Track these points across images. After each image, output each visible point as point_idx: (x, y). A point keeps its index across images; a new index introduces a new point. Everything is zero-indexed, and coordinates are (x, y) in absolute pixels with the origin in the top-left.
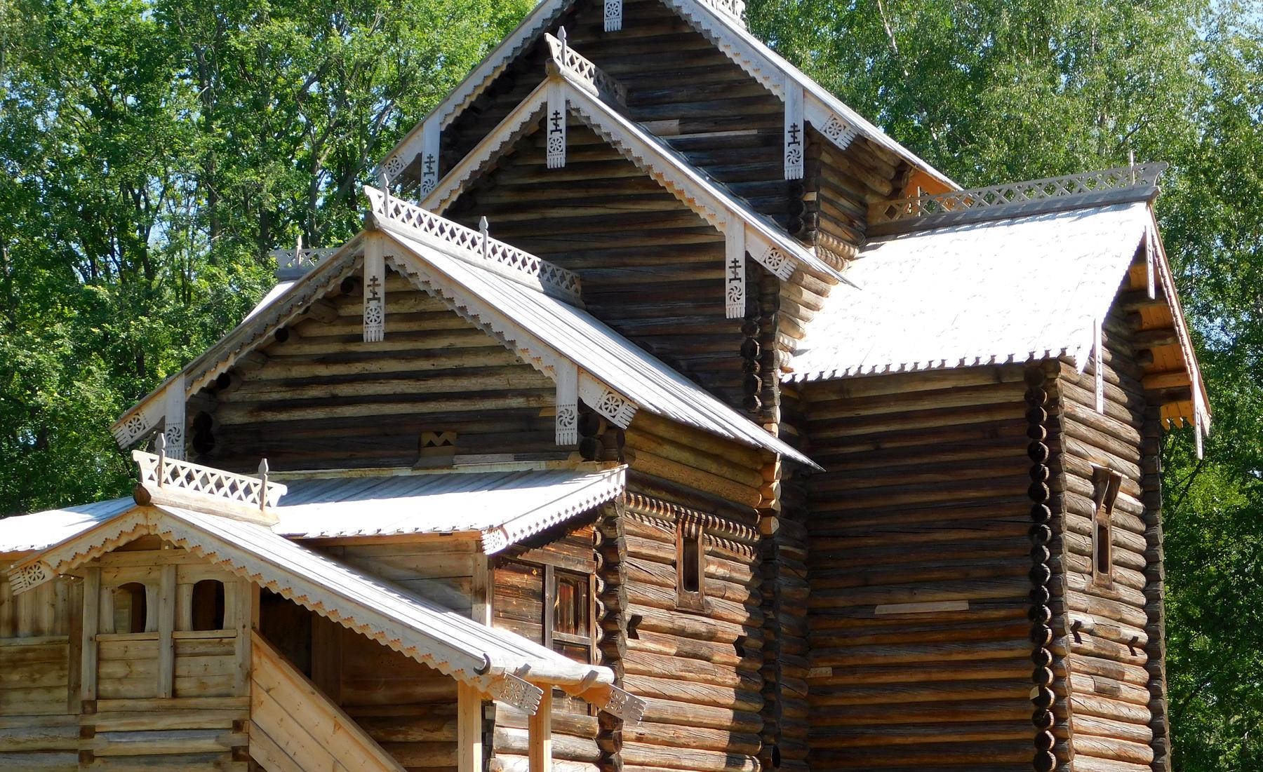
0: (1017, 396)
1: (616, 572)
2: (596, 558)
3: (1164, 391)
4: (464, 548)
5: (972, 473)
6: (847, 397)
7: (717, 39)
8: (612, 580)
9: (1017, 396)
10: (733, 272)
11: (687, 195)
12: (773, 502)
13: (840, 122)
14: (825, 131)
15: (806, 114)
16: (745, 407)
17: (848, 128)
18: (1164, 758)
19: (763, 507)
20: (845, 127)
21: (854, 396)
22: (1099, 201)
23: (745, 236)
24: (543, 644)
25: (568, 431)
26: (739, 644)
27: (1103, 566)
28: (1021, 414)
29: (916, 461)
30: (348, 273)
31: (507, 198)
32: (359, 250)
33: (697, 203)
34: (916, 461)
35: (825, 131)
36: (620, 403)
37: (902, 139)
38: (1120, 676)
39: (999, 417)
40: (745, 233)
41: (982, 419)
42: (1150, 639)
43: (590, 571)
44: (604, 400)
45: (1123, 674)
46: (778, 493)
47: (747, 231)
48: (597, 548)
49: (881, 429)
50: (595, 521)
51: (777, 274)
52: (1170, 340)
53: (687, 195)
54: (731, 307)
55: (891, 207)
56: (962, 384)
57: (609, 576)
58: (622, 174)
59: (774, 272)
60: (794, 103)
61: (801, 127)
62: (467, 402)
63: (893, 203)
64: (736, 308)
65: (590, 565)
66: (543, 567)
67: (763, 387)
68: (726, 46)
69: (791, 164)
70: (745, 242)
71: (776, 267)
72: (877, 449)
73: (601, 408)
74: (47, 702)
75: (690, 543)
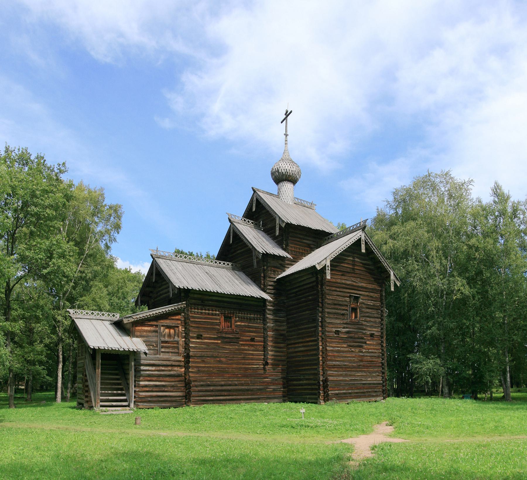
9: (314, 279)
28: (314, 284)
38: (365, 343)
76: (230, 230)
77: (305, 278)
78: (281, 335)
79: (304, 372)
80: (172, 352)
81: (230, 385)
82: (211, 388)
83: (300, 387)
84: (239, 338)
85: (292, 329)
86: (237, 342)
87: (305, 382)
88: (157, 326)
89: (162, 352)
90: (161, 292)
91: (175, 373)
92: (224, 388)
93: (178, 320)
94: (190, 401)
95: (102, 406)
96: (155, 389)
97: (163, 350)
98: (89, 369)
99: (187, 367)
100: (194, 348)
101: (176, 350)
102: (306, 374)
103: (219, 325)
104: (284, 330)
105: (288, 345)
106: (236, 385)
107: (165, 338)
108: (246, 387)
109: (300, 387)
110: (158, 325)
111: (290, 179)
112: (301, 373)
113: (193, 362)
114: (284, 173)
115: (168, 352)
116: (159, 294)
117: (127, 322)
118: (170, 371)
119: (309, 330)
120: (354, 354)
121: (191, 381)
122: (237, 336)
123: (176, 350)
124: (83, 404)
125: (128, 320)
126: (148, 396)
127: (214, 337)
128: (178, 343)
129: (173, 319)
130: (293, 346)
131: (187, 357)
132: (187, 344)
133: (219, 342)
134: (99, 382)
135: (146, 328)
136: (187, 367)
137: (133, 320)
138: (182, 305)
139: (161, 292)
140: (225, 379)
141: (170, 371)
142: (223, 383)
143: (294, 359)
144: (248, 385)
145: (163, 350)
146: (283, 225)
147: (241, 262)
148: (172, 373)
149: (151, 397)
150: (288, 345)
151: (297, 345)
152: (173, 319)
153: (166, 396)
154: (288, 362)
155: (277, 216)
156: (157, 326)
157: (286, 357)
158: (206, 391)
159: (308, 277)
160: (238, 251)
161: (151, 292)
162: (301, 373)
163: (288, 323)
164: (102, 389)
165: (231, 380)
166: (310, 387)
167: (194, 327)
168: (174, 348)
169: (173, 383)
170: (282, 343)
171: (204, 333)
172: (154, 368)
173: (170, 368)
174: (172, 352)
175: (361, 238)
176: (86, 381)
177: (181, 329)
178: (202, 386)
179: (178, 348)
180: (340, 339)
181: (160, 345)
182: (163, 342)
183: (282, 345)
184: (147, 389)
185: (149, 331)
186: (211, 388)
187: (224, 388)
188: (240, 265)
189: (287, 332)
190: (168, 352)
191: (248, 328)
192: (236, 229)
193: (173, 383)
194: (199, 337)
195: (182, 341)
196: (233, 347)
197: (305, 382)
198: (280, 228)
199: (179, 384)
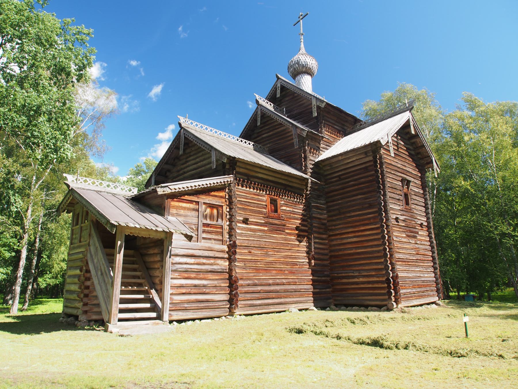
5: (363, 180)
9: (371, 158)
16: (300, 170)
18: (435, 254)
21: (334, 166)
26: (297, 228)
27: (407, 203)
28: (372, 163)
31: (256, 135)
37: (432, 165)
38: (417, 233)
39: (368, 165)
42: (428, 224)
45: (418, 232)
49: (340, 173)
52: (424, 149)
58: (276, 124)
62: (354, 228)
67: (305, 164)
72: (340, 178)
74: (103, 263)
75: (274, 202)
76: (257, 112)
77: (354, 159)
78: (323, 224)
79: (360, 268)
80: (215, 240)
81: (278, 284)
82: (259, 288)
83: (353, 286)
84: (284, 226)
85: (336, 218)
86: (284, 230)
87: (361, 279)
88: (197, 203)
89: (204, 238)
90: (186, 170)
91: (219, 267)
92: (272, 288)
93: (221, 197)
94: (237, 306)
95: (120, 320)
96: (193, 291)
97: (204, 235)
98: (95, 261)
99: (231, 260)
100: (241, 235)
101: (220, 237)
102: (362, 270)
103: (265, 208)
104: (324, 219)
105: (330, 236)
106: (284, 284)
107: (207, 220)
108: (294, 287)
109: (353, 286)
110: (199, 202)
111: (309, 71)
112: (354, 268)
113: (241, 254)
114: (304, 65)
115: (210, 239)
116: (181, 172)
117: (162, 193)
118: (211, 264)
119: (366, 217)
120: (411, 246)
121: (238, 279)
122: (283, 222)
123: (220, 237)
124: (76, 317)
125: (164, 191)
126: (184, 301)
127: (261, 223)
128: (222, 227)
129: (216, 196)
130: (338, 237)
131: (233, 248)
132: (231, 229)
133: (266, 229)
134: (118, 280)
135: (181, 204)
136: (231, 260)
137: (170, 191)
138: (229, 178)
139: (186, 170)
140: (272, 276)
141: (211, 264)
142: (271, 282)
143: (340, 253)
144: (295, 284)
145: (204, 235)
146: (323, 105)
147: (268, 145)
148: (215, 267)
149: (189, 302)
150: (330, 236)
151: (344, 236)
152: (216, 196)
153: (207, 301)
154: (331, 257)
155: (313, 97)
156: (197, 203)
157: (328, 251)
158: (253, 292)
159: (358, 158)
160: (263, 134)
161: (169, 171)
162: (354, 268)
163: (329, 211)
164: (122, 292)
165: (279, 277)
166: (370, 286)
167: (240, 209)
168: (217, 233)
169: (216, 282)
170: (323, 234)
171: (251, 217)
172: (192, 260)
173: (212, 261)
174: (215, 240)
175: (409, 119)
176: (89, 279)
177: (226, 209)
178: (249, 285)
179: (222, 234)
180: (400, 228)
181: (201, 229)
182: (205, 225)
183: (324, 236)
184: (184, 291)
185: (189, 209)
186: (259, 288)
187: (272, 288)
188: (267, 149)
189: (328, 221)
190: (210, 239)
191: (294, 214)
192: (265, 110)
193: (216, 282)
194: (246, 221)
195: (226, 224)
196: (280, 236)
197: (361, 279)
198: (318, 108)
199: (222, 283)
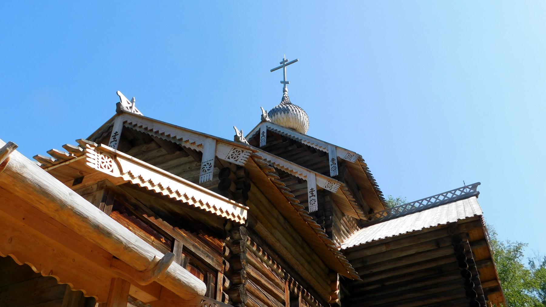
0: (449, 251)
1: (239, 274)
2: (224, 263)
3: (487, 289)
4: (89, 192)
6: (366, 265)
7: (301, 140)
8: (236, 280)
9: (449, 251)
10: (311, 194)
11: (290, 169)
12: (337, 300)
13: (351, 154)
14: (346, 158)
15: (337, 154)
17: (355, 155)
19: (333, 302)
20: (354, 155)
22: (455, 199)
23: (316, 179)
24: (103, 212)
25: (207, 174)
28: (453, 260)
29: (404, 288)
30: (105, 135)
32: (112, 123)
33: (294, 171)
34: (404, 288)
35: (346, 158)
36: (241, 152)
40: (316, 178)
41: (433, 265)
43: (219, 269)
44: (231, 153)
46: (339, 296)
47: (316, 177)
48: (226, 258)
49: (383, 276)
50: (225, 239)
51: (331, 191)
52: (489, 263)
53: (290, 169)
54: (311, 208)
55: (370, 217)
56: (420, 250)
57: (234, 278)
59: (330, 190)
60: (332, 152)
61: (336, 159)
63: (371, 215)
64: (314, 207)
65: (220, 265)
66: (173, 240)
68: (304, 141)
69: (333, 171)
70: (316, 181)
71: (331, 188)
73: (229, 158)
